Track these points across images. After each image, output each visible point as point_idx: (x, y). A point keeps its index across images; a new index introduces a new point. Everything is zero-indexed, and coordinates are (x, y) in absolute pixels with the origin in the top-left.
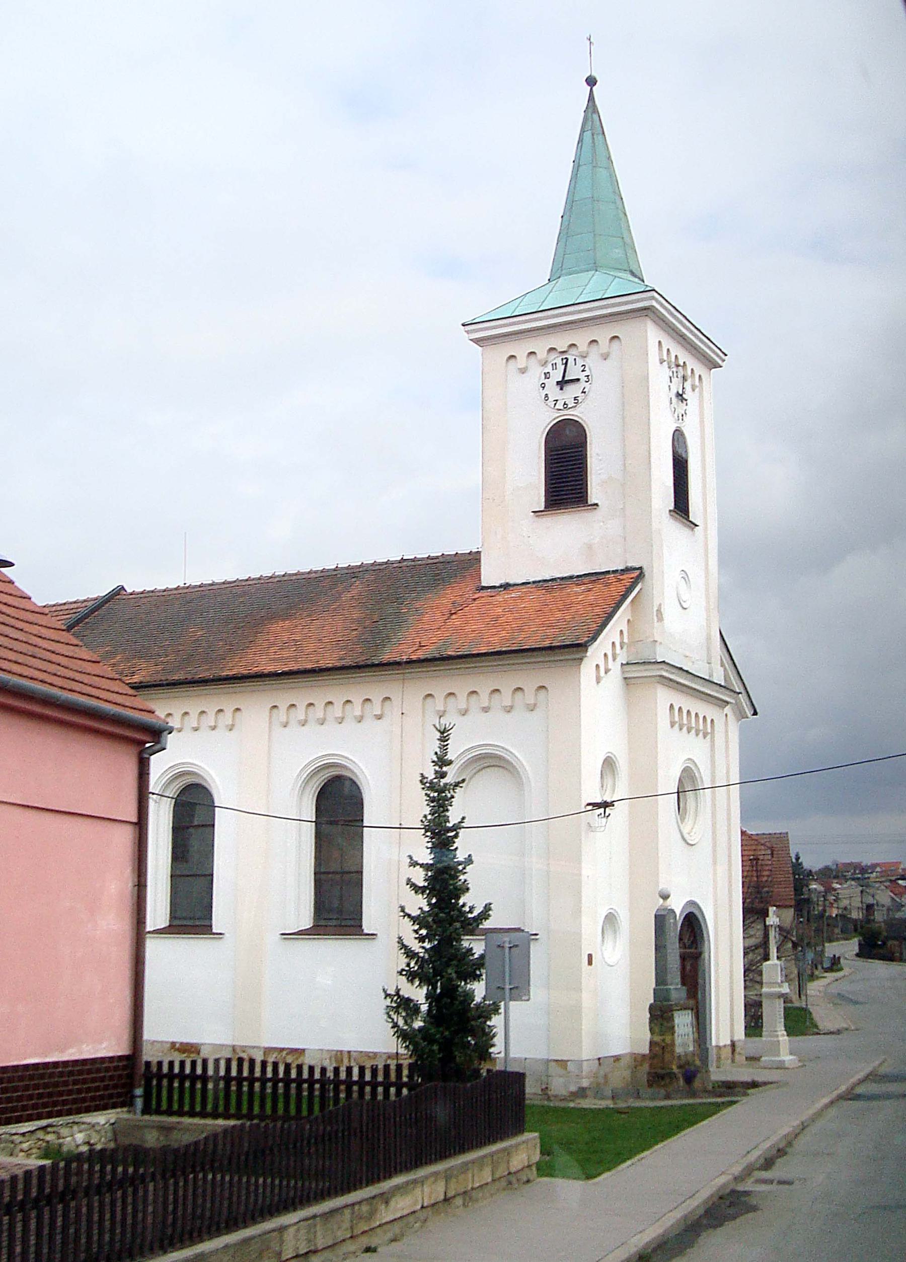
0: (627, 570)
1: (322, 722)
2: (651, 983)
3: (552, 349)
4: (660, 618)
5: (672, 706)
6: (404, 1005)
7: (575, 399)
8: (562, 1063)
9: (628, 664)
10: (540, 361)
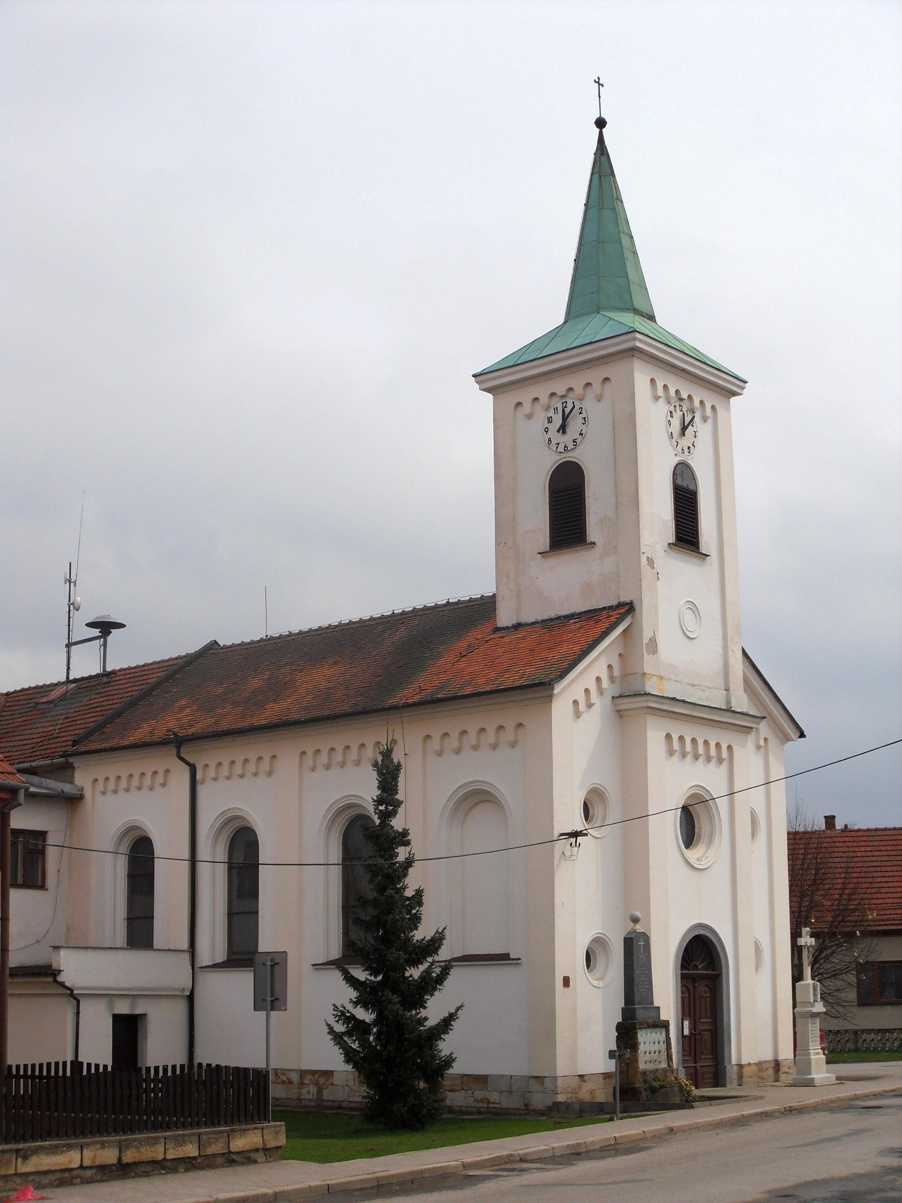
0: (620, 605)
1: (494, 747)
2: (620, 1002)
5: (668, 736)
6: (358, 1028)
7: (574, 441)
8: (540, 1079)
9: (621, 696)
10: (543, 406)
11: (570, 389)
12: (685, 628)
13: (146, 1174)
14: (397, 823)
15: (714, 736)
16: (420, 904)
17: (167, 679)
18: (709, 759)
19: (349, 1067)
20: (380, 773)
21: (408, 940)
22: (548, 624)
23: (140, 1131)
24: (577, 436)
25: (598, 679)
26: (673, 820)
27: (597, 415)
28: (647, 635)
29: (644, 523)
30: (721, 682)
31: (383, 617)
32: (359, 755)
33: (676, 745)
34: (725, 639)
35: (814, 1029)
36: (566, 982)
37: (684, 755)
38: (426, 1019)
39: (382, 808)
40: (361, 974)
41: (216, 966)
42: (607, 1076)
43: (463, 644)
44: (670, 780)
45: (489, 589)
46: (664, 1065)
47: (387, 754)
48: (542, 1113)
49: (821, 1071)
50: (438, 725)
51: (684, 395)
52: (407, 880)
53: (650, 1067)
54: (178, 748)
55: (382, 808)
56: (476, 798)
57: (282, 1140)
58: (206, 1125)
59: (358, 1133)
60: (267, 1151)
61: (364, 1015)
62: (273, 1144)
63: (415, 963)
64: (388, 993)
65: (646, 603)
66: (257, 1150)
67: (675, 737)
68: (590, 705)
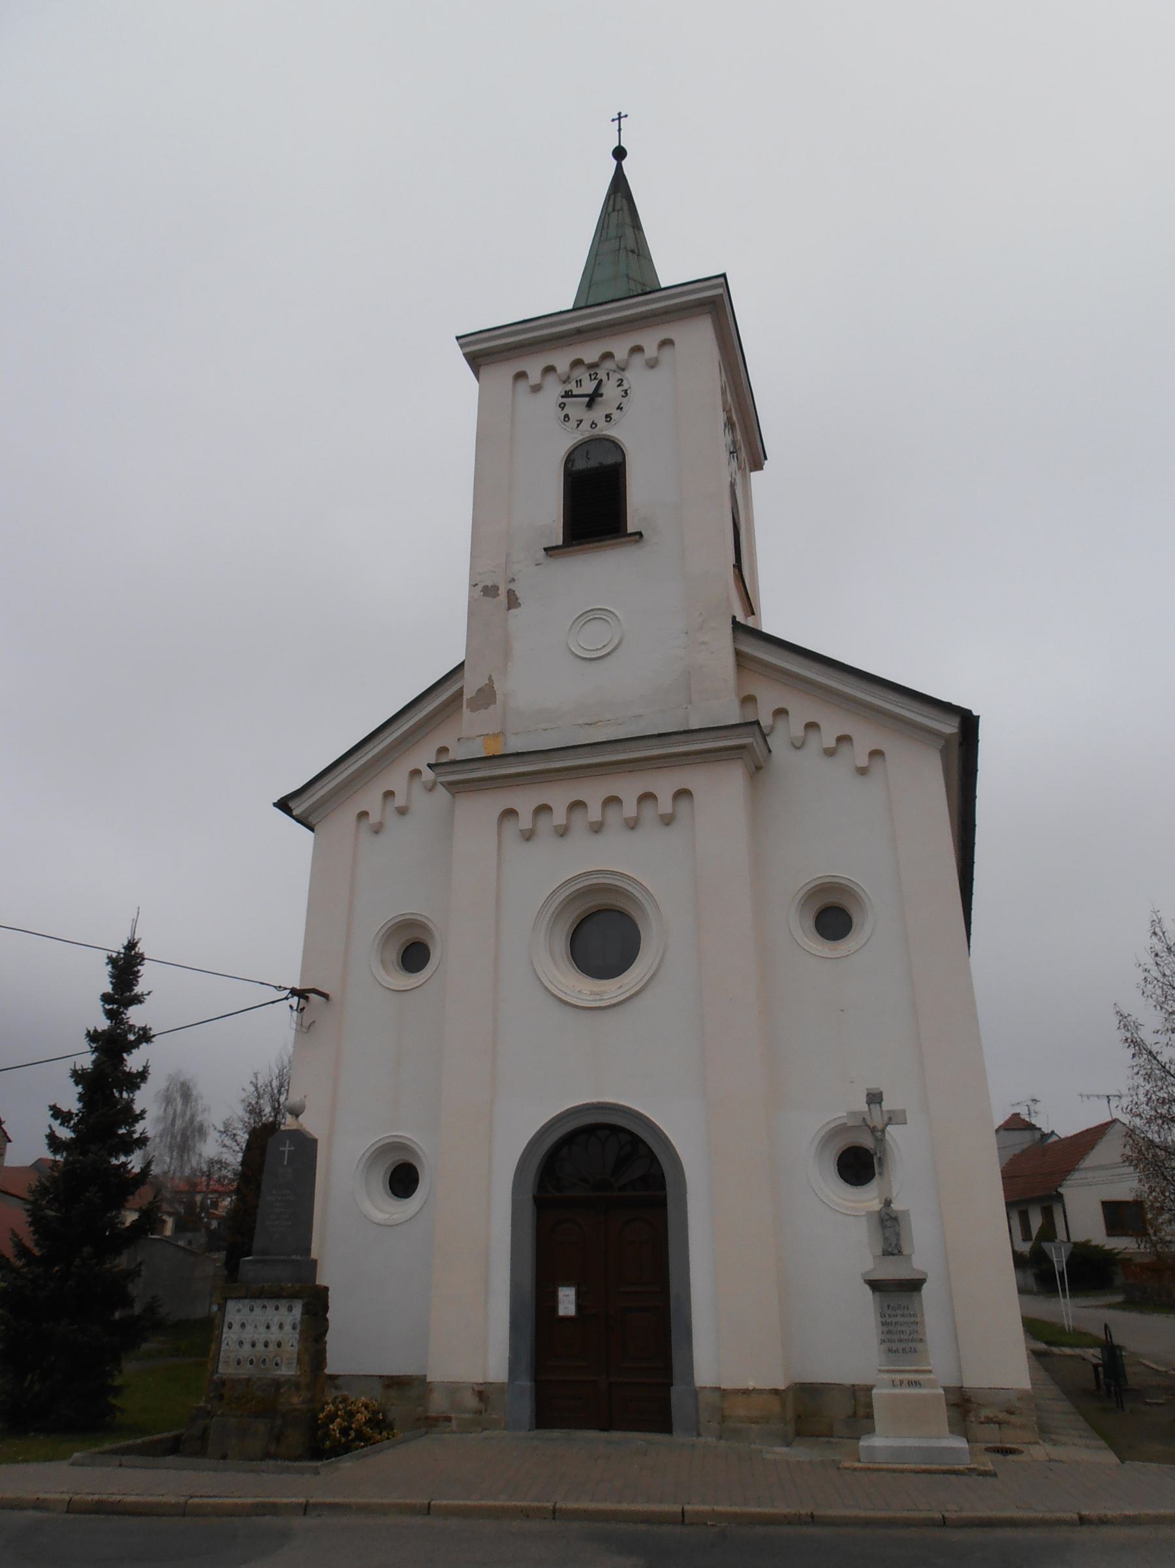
11: (608, 356)
45: (752, 474)
53: (245, 1372)
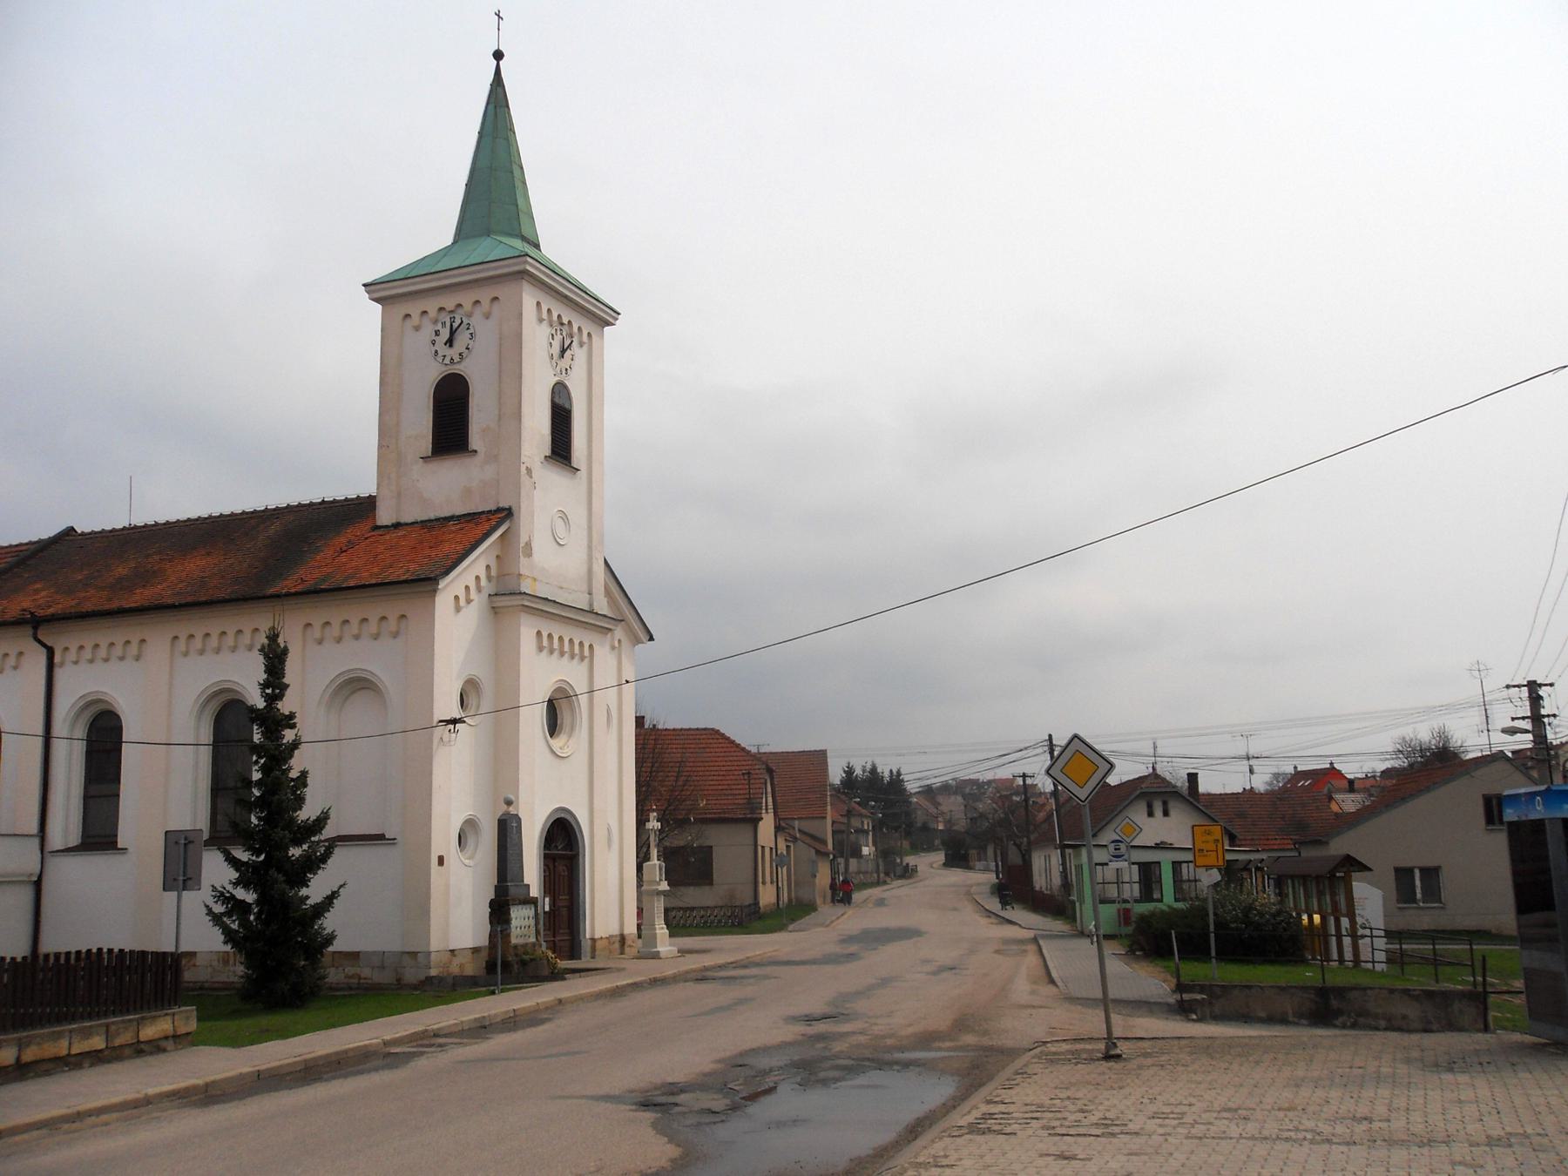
0: (499, 510)
2: (491, 880)
3: (441, 309)
4: (529, 554)
5: (539, 633)
6: (238, 907)
12: (556, 538)
13: (47, 1073)
14: (285, 707)
15: (578, 635)
16: (305, 785)
17: (18, 564)
18: (572, 657)
19: (228, 948)
20: (266, 656)
21: (293, 820)
22: (427, 525)
23: (43, 1026)
24: (463, 349)
25: (478, 578)
26: (540, 712)
27: (484, 332)
28: (523, 539)
29: (525, 434)
30: (585, 587)
31: (255, 512)
32: (252, 639)
33: (545, 643)
34: (590, 547)
35: (659, 906)
36: (441, 861)
37: (551, 652)
38: (307, 897)
39: (269, 691)
40: (242, 855)
41: (68, 850)
42: (476, 950)
43: (342, 540)
44: (539, 674)
46: (533, 939)
47: (273, 637)
48: (415, 987)
49: (665, 944)
50: (318, 614)
51: (565, 321)
52: (293, 762)
53: (521, 941)
54: (35, 628)
55: (269, 691)
56: (357, 685)
57: (192, 1026)
58: (114, 1014)
59: (235, 1014)
60: (176, 1037)
61: (249, 897)
62: (182, 1030)
63: (298, 843)
64: (273, 872)
65: (523, 506)
66: (166, 1038)
67: (545, 635)
68: (469, 601)
